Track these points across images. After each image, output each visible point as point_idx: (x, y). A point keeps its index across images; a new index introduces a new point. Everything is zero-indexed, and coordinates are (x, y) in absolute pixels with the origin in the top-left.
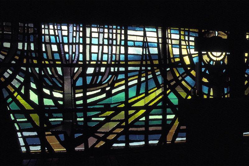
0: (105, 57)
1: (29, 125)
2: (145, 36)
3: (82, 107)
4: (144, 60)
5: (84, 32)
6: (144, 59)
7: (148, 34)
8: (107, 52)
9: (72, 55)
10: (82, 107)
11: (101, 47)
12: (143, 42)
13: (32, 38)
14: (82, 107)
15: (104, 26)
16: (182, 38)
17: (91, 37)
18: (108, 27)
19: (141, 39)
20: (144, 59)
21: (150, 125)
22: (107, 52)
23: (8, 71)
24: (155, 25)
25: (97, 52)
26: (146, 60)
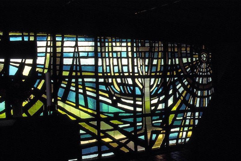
0: (125, 69)
1: (88, 136)
2: (76, 46)
3: (132, 113)
4: (74, 71)
5: (54, 41)
6: (74, 69)
7: (80, 44)
8: (127, 64)
9: (106, 68)
10: (140, 114)
11: (119, 60)
12: (75, 52)
13: (176, 56)
14: (140, 114)
15: (127, 40)
16: (156, 50)
17: (127, 52)
18: (23, 34)
19: (72, 50)
20: (74, 69)
21: (193, 124)
22: (127, 64)
23: (184, 81)
24: (88, 35)
25: (43, 63)
26: (76, 71)
